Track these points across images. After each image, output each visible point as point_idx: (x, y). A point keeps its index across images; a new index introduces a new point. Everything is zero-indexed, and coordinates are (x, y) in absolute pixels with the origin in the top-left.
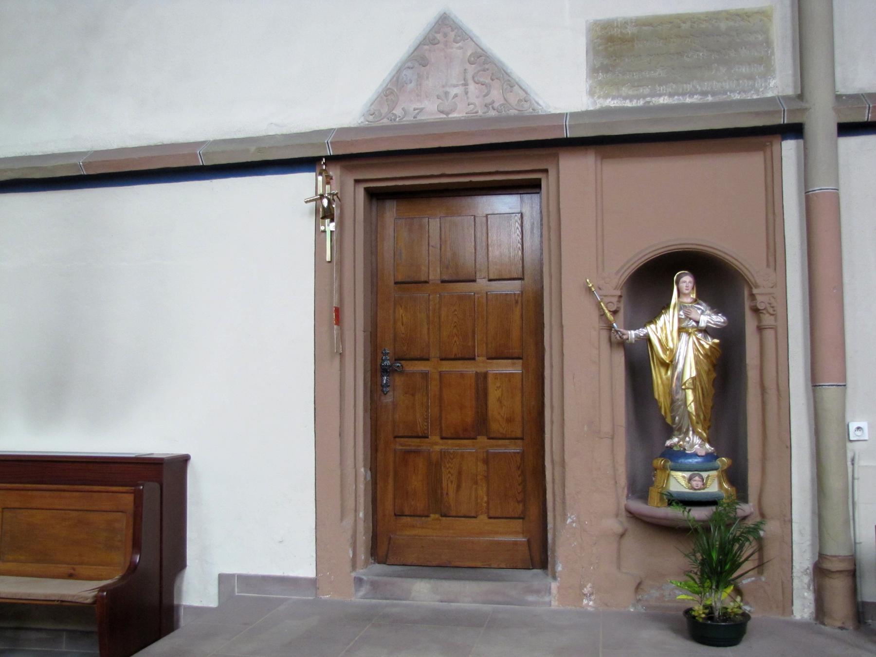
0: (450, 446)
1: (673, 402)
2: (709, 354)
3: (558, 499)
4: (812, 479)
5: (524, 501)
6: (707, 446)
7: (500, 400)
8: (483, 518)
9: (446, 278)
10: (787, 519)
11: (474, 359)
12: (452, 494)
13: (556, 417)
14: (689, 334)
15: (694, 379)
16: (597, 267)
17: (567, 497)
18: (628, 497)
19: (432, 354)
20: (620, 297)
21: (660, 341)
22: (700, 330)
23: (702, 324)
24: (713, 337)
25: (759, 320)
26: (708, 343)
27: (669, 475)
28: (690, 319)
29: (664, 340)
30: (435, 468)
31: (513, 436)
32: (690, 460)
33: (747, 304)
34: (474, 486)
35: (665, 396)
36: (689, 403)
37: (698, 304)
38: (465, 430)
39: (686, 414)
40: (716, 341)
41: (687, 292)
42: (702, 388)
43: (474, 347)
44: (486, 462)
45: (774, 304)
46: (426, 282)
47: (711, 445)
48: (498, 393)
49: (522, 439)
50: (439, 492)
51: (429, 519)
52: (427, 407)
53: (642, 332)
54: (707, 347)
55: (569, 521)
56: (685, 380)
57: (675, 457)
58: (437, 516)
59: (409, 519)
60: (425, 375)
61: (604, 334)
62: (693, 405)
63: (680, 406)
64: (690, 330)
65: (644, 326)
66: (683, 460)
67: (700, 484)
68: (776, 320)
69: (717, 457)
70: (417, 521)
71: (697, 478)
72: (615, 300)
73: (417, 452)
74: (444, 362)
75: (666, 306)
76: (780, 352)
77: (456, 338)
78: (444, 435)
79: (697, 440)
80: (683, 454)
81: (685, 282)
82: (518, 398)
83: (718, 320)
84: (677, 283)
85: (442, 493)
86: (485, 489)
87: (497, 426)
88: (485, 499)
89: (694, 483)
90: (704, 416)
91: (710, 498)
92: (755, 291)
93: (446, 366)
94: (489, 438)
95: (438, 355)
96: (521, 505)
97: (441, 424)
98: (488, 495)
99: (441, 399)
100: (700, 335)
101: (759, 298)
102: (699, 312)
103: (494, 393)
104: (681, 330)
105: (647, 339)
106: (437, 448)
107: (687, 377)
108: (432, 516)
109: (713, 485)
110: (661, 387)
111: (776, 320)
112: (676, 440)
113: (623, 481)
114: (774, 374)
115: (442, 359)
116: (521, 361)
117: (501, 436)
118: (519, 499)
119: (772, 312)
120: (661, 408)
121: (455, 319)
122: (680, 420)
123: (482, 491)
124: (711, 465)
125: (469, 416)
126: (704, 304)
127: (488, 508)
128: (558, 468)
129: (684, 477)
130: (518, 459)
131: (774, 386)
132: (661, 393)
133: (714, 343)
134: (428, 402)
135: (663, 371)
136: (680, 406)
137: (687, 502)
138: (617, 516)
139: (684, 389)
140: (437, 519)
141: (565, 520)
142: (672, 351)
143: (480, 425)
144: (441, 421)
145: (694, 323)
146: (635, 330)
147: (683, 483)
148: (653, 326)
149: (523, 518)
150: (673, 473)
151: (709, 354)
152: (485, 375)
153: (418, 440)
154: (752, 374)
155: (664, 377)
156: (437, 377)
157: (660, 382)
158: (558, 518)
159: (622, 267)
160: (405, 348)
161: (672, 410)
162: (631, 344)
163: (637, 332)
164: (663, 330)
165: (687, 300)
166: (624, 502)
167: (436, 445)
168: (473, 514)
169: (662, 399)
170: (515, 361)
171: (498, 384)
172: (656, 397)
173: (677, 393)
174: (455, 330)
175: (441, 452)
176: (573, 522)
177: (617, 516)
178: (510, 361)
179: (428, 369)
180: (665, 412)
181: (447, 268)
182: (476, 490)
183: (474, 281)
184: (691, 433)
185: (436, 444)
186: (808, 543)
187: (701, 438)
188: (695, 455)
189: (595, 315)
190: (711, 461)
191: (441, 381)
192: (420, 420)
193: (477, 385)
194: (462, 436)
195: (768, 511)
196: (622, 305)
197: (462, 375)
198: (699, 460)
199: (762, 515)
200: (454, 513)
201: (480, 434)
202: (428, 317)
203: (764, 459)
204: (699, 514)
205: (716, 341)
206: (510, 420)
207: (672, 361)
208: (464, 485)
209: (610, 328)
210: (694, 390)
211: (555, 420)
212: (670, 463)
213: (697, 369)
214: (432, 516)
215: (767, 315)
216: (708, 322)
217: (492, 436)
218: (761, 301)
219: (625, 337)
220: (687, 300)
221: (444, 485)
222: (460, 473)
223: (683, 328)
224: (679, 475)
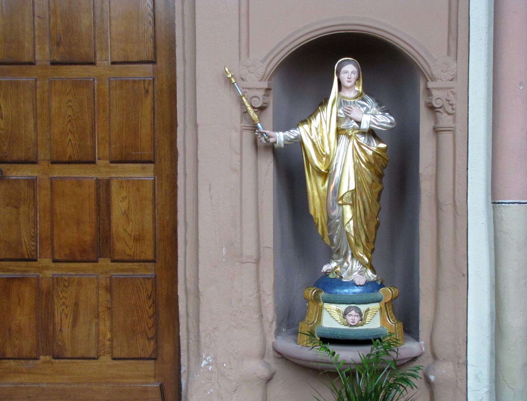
0: (64, 270)
1: (329, 219)
2: (373, 161)
3: (192, 336)
4: (491, 313)
5: (156, 338)
6: (369, 273)
7: (126, 214)
8: (106, 359)
9: (57, 59)
10: (461, 361)
11: (94, 162)
12: (66, 330)
13: (190, 238)
14: (350, 137)
15: (354, 192)
16: (240, 53)
17: (203, 335)
18: (278, 332)
19: (41, 156)
20: (268, 90)
21: (314, 145)
22: (363, 133)
23: (365, 126)
24: (379, 140)
25: (436, 121)
26: (376, 146)
27: (321, 310)
28: (351, 119)
29: (319, 144)
30: (45, 298)
31: (142, 258)
32: (346, 291)
33: (422, 101)
34: (95, 321)
35: (322, 212)
36: (346, 221)
37: (363, 100)
38: (84, 251)
39: (345, 234)
40: (382, 145)
41: (349, 84)
42: (363, 203)
43: (94, 148)
44: (109, 289)
45: (453, 101)
46: (31, 64)
47: (374, 271)
48: (124, 205)
49: (154, 261)
50: (51, 328)
51: (38, 362)
52: (35, 223)
53: (292, 134)
54: (370, 153)
55: (204, 363)
56: (342, 194)
57: (329, 286)
58: (48, 358)
59: (12, 363)
60: (32, 183)
61: (248, 136)
62: (352, 223)
63: (337, 224)
64: (350, 133)
65: (296, 127)
66: (338, 291)
67: (357, 319)
68: (454, 121)
69: (382, 286)
70: (23, 365)
71: (353, 312)
72: (260, 94)
73: (22, 280)
74: (57, 166)
75: (323, 102)
76: (458, 161)
77: (70, 136)
78: (57, 257)
79: (356, 266)
80: (339, 283)
81: (346, 72)
82: (149, 211)
83: (384, 120)
84: (338, 73)
85: (54, 329)
86: (108, 323)
87: (122, 246)
88: (109, 336)
89: (349, 318)
90: (367, 238)
91: (367, 336)
92: (430, 85)
93: (59, 171)
94: (113, 261)
95: (48, 157)
96: (152, 343)
97: (52, 244)
98: (111, 331)
99: (52, 212)
100: (362, 139)
101: (435, 93)
102: (363, 109)
103: (119, 205)
104: (339, 132)
105: (299, 142)
106: (49, 273)
107: (344, 190)
108: (42, 358)
109: (374, 319)
110: (317, 200)
111: (454, 121)
112: (334, 264)
113: (270, 314)
114: (451, 187)
115: (53, 163)
116: (152, 165)
117: (127, 258)
118: (150, 336)
119: (450, 111)
120: (317, 225)
121: (70, 112)
122: (338, 241)
123: (105, 327)
124: (372, 296)
125: (88, 233)
126: (370, 100)
127: (112, 347)
128: (191, 298)
129: (338, 311)
130: (149, 286)
131: (451, 201)
132: (318, 208)
133: (379, 149)
134: (35, 215)
135: (320, 181)
136: (337, 224)
137: (331, 340)
138: (262, 356)
139: (342, 205)
140: (49, 362)
141: (200, 362)
142: (328, 157)
143: (102, 244)
144: (52, 239)
145: (355, 124)
146: (284, 131)
147: (338, 317)
148: (306, 126)
149: (155, 359)
150: (326, 305)
151: (373, 161)
152: (108, 183)
153: (24, 264)
154: (426, 187)
155: (321, 188)
156: (48, 184)
157: (316, 194)
158: (193, 359)
159: (273, 51)
160: (5, 148)
161: (329, 228)
162: (280, 148)
163: (287, 133)
164: (318, 133)
165: (350, 94)
166: (271, 339)
167: (48, 270)
168: (93, 354)
169: (318, 215)
170: (145, 165)
171: (124, 194)
172: (312, 212)
173: (334, 209)
174: (69, 126)
175: (53, 278)
176: (209, 364)
177: (262, 356)
178: (139, 165)
179: (36, 174)
180: (323, 232)
181: (58, 44)
182: (97, 324)
183: (93, 64)
184: (350, 256)
185: (47, 268)
186: (486, 389)
187: (362, 262)
188: (353, 284)
189: (236, 112)
190: (373, 291)
191: (52, 191)
192: (25, 239)
193: (98, 195)
194: (79, 258)
195: (439, 351)
196: (270, 100)
197: (79, 182)
198: (357, 290)
199: (435, 357)
200: (69, 355)
201: (102, 255)
202: (35, 108)
203: (437, 289)
204: (348, 355)
205: (382, 145)
206: (138, 239)
207: (328, 170)
208: (81, 319)
209: (256, 128)
210: (353, 206)
211: (189, 238)
212: (322, 294)
213: (356, 180)
214: (42, 358)
215: (445, 115)
216: (371, 122)
217: (116, 258)
218: (438, 98)
219: (271, 140)
220: (350, 94)
221: (57, 319)
222: (76, 304)
223: (343, 130)
224: (334, 307)
